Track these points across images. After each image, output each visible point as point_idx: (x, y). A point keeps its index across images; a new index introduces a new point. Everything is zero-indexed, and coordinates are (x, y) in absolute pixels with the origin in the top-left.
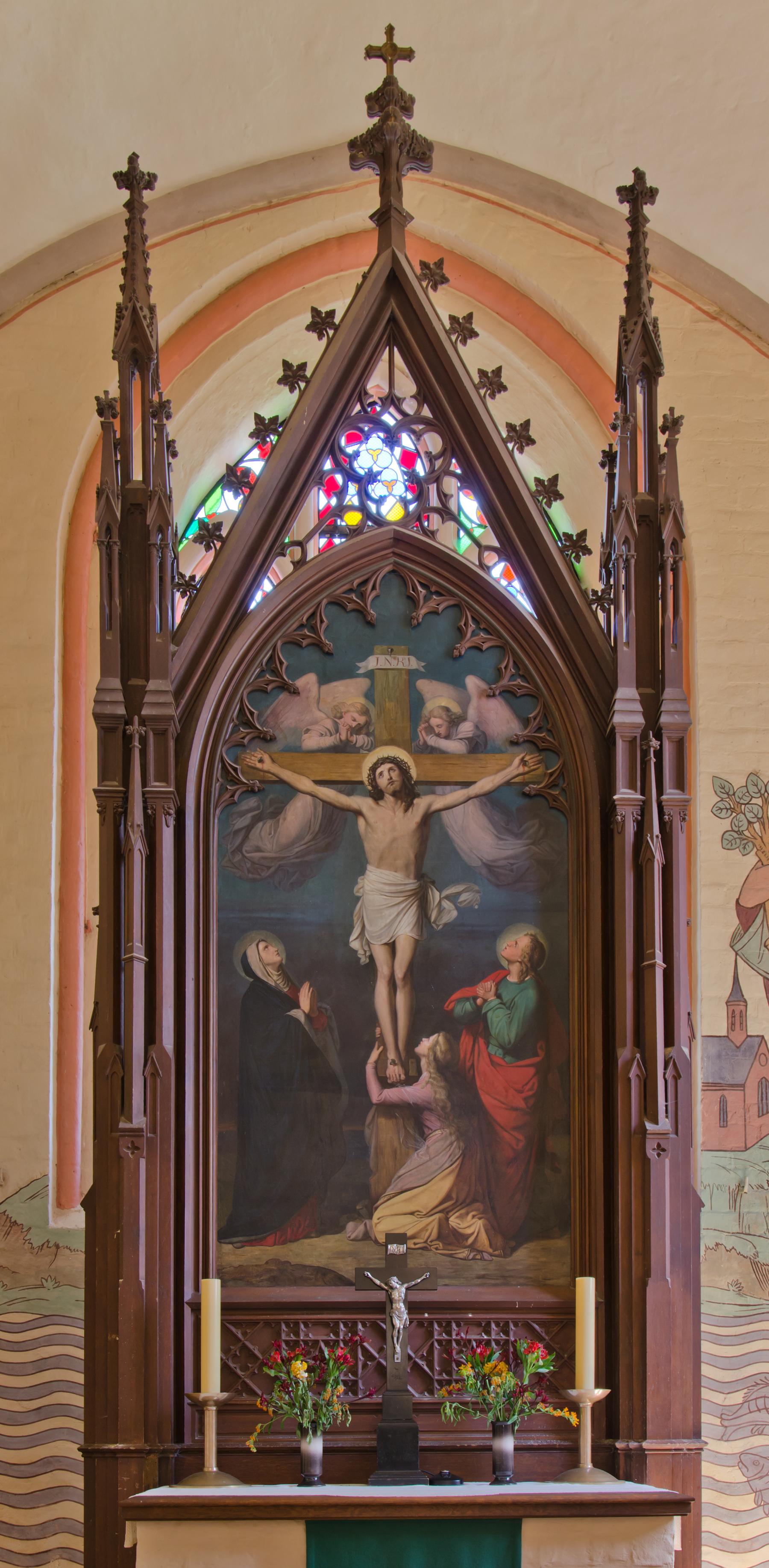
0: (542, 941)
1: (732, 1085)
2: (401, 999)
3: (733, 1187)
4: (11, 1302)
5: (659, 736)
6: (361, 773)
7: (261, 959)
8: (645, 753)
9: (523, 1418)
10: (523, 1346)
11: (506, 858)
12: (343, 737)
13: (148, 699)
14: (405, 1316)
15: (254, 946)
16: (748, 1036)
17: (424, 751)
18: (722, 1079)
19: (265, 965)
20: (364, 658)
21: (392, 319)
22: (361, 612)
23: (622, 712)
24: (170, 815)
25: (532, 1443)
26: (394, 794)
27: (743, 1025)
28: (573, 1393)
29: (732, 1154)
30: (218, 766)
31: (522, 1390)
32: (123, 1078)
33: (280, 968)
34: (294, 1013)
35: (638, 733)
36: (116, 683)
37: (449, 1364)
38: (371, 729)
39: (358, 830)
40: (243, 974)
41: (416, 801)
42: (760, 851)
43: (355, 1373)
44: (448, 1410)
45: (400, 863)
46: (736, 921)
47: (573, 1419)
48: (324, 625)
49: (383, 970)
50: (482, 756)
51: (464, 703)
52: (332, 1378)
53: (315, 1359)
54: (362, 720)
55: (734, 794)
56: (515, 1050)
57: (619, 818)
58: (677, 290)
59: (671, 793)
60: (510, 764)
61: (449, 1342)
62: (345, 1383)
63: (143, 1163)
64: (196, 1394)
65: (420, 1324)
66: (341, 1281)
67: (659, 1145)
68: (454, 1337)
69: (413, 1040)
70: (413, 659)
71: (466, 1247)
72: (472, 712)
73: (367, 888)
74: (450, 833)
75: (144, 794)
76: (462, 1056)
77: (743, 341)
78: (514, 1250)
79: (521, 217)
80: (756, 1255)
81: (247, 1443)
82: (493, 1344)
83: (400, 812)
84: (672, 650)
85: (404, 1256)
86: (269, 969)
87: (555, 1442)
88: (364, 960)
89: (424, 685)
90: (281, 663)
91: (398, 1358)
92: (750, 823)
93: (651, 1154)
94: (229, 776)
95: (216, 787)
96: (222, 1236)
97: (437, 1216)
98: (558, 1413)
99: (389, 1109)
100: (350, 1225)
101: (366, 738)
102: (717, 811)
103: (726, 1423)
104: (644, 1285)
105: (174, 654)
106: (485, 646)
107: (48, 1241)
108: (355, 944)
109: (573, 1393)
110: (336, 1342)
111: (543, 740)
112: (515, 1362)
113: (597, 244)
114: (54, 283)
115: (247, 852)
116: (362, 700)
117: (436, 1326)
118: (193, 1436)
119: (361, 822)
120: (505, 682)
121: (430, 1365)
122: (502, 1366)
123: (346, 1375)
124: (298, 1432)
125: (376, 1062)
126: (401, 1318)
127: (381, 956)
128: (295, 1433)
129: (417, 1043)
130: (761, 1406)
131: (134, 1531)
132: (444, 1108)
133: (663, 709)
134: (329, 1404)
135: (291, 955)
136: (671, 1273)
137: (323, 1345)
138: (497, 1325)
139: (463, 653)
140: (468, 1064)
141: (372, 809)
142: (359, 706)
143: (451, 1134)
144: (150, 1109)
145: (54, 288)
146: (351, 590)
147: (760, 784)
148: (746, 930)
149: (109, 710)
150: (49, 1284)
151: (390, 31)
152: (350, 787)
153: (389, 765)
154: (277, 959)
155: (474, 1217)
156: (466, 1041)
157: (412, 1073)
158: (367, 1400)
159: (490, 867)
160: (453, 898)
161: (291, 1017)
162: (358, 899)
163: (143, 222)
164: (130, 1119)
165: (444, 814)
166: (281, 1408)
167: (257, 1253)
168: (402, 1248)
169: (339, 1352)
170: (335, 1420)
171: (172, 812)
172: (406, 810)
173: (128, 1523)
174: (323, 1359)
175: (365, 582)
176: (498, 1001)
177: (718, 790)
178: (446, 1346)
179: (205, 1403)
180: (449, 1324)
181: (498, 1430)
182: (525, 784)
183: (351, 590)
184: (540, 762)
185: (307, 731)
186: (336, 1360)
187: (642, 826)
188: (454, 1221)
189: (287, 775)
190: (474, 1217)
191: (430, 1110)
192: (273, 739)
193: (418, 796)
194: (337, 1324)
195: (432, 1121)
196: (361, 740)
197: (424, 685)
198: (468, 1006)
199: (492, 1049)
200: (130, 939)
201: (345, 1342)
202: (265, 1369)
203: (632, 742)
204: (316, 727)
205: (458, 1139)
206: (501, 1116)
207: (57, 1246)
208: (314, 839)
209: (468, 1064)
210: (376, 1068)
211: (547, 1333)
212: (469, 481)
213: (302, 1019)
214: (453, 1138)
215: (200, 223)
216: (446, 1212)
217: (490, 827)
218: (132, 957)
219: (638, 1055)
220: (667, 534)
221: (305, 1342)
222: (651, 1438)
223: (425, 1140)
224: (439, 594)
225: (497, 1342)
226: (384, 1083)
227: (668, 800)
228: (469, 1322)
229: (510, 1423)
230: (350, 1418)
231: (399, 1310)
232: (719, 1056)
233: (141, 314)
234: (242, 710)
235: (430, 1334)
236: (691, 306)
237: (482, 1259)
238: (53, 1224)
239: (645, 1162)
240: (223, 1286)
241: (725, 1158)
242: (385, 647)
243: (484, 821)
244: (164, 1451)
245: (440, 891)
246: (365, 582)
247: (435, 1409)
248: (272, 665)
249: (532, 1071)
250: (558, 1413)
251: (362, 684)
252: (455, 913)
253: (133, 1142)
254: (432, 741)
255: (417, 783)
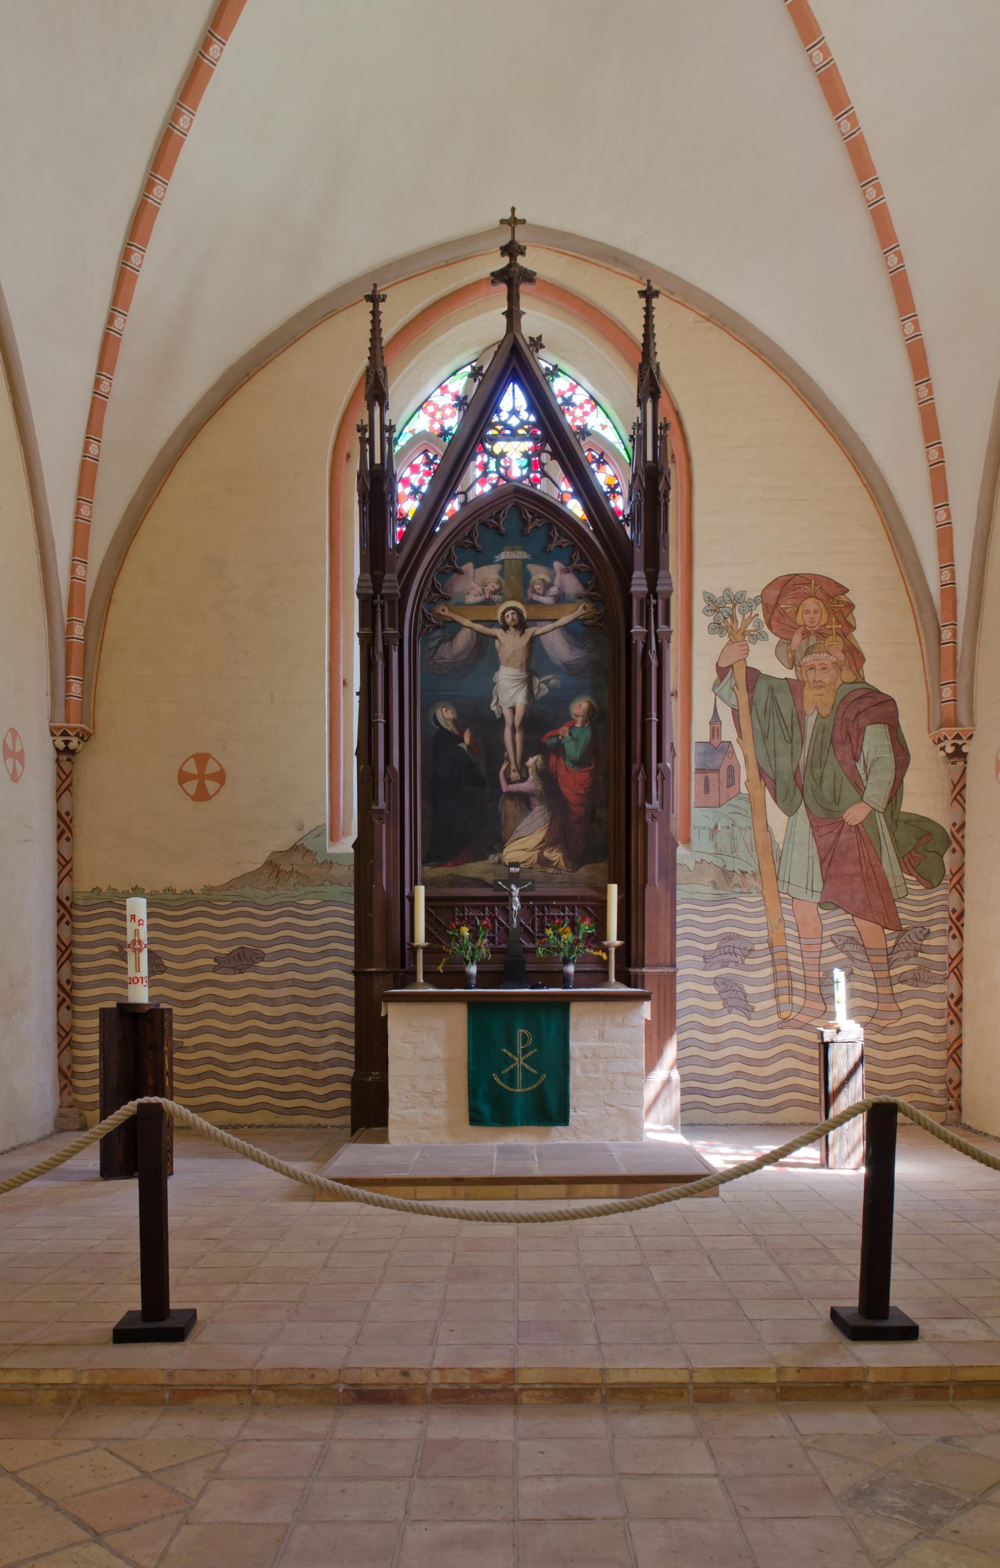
0: (594, 705)
1: (711, 770)
2: (518, 737)
3: (712, 828)
4: (306, 894)
5: (656, 597)
6: (497, 616)
7: (443, 717)
8: (648, 607)
9: (579, 956)
10: (578, 920)
11: (574, 660)
12: (487, 597)
13: (384, 585)
14: (519, 904)
15: (440, 710)
16: (722, 742)
17: (530, 603)
18: (707, 766)
19: (446, 720)
20: (499, 553)
21: (514, 369)
22: (497, 529)
23: (636, 585)
24: (396, 645)
25: (586, 969)
26: (515, 627)
27: (719, 735)
28: (606, 943)
29: (711, 809)
30: (420, 615)
31: (577, 941)
32: (373, 783)
33: (454, 721)
34: (461, 745)
35: (644, 596)
36: (368, 576)
37: (542, 928)
38: (502, 592)
39: (495, 647)
40: (434, 725)
41: (526, 630)
42: (731, 634)
43: (494, 933)
44: (540, 952)
45: (518, 664)
46: (716, 676)
47: (605, 957)
48: (477, 537)
49: (508, 721)
50: (561, 605)
51: (553, 576)
52: (481, 936)
53: (472, 926)
54: (497, 587)
55: (716, 601)
56: (579, 763)
57: (634, 642)
58: (685, 303)
59: (662, 628)
60: (577, 609)
61: (543, 917)
62: (488, 938)
63: (384, 826)
64: (412, 944)
65: (528, 907)
66: (486, 885)
67: (652, 816)
68: (546, 914)
69: (525, 758)
70: (525, 553)
71: (552, 867)
72: (557, 581)
73: (500, 678)
74: (545, 647)
75: (383, 634)
76: (551, 767)
77: (725, 333)
78: (578, 869)
79: (593, 265)
80: (725, 866)
81: (439, 968)
82: (567, 918)
83: (517, 637)
84: (664, 550)
85: (517, 874)
86: (448, 722)
87: (598, 969)
88: (498, 716)
89: (531, 567)
90: (454, 558)
91: (515, 925)
92: (725, 618)
93: (649, 820)
94: (426, 619)
95: (419, 626)
96: (424, 862)
97: (537, 851)
98: (596, 953)
99: (511, 795)
100: (491, 856)
101: (500, 597)
102: (706, 612)
103: (707, 961)
104: (644, 888)
105: (398, 557)
106: (564, 545)
107: (326, 860)
108: (493, 708)
109: (606, 943)
110: (484, 917)
111: (595, 596)
112: (574, 927)
113: (638, 279)
114: (325, 316)
115: (436, 659)
116: (497, 576)
117: (536, 909)
118: (410, 965)
119: (497, 642)
120: (574, 565)
121: (533, 929)
122: (568, 929)
123: (489, 933)
124: (464, 963)
125: (505, 771)
126: (516, 906)
127: (507, 713)
128: (462, 964)
129: (527, 760)
130: (727, 951)
131: (386, 1008)
132: (541, 795)
133: (658, 582)
134: (480, 948)
135: (459, 713)
136: (659, 880)
137: (477, 918)
138: (569, 908)
139: (552, 549)
140: (554, 771)
141: (503, 635)
142: (496, 580)
143: (545, 808)
144: (387, 799)
145: (324, 318)
146: (491, 517)
147: (731, 595)
148: (722, 680)
149: (364, 591)
150: (327, 883)
151: (513, 210)
152: (491, 623)
153: (512, 611)
154: (452, 716)
155: (557, 851)
156: (553, 759)
157: (524, 776)
158: (500, 946)
159: (566, 665)
160: (546, 682)
161: (459, 747)
162: (495, 683)
163: (380, 321)
164: (377, 804)
165: (542, 637)
166: (455, 950)
167: (442, 870)
168: (518, 870)
169: (485, 922)
170: (483, 956)
171: (397, 643)
172: (521, 635)
173: (383, 1004)
174: (477, 926)
175: (499, 512)
176: (570, 737)
177: (707, 599)
178: (541, 918)
179: (417, 948)
180: (543, 907)
181: (566, 961)
182: (585, 620)
183: (491, 517)
184: (593, 608)
185: (468, 594)
186: (483, 927)
187: (646, 646)
188: (546, 854)
189: (457, 618)
190: (557, 851)
191: (533, 795)
192: (450, 599)
193: (527, 627)
194: (484, 907)
195: (534, 801)
196: (496, 598)
197: (531, 567)
198: (554, 740)
199: (567, 763)
200: (376, 711)
201: (489, 917)
202: (448, 931)
203: (642, 601)
204: (473, 591)
205: (548, 811)
206: (572, 798)
207: (331, 863)
208: (471, 652)
209: (554, 771)
210: (505, 774)
211: (595, 912)
212: (555, 455)
213: (465, 748)
214: (546, 810)
215: (407, 276)
216: (542, 849)
217: (567, 644)
218: (377, 722)
219: (642, 768)
220: (661, 487)
221: (468, 917)
222: (648, 966)
223: (531, 811)
224: (539, 518)
225: (569, 917)
226: (509, 781)
227: (659, 632)
228: (554, 906)
229: (571, 958)
230: (490, 955)
231: (515, 901)
232: (705, 753)
233: (380, 375)
234: (433, 584)
235: (533, 912)
236: (694, 313)
237: (561, 873)
238: (330, 850)
239: (646, 825)
240: (426, 888)
241: (708, 812)
242: (510, 547)
243: (564, 640)
244: (395, 972)
245: (539, 679)
246: (499, 512)
247: (533, 951)
248: (449, 560)
249: (588, 774)
250: (596, 953)
251: (497, 567)
252: (547, 691)
253: (379, 816)
254: (535, 597)
255: (526, 620)
